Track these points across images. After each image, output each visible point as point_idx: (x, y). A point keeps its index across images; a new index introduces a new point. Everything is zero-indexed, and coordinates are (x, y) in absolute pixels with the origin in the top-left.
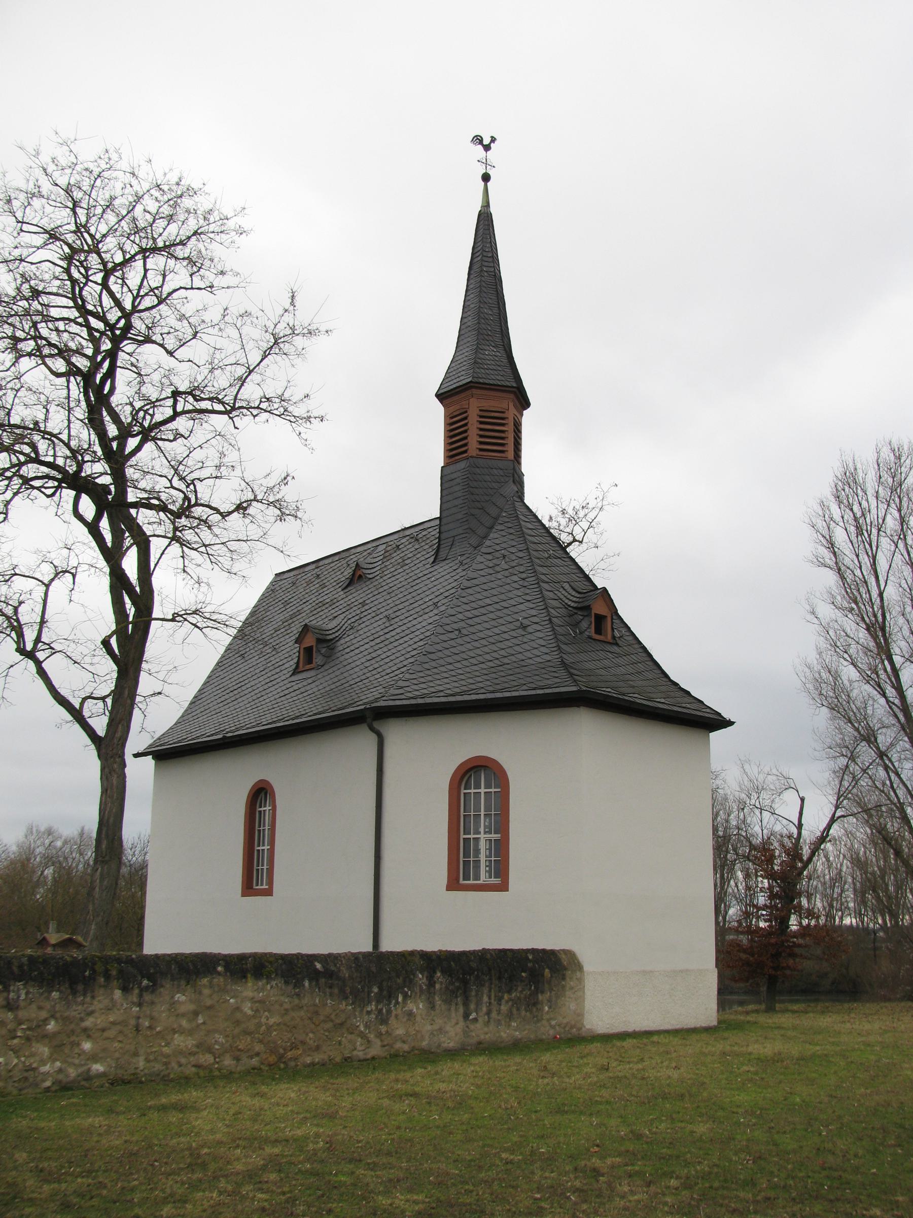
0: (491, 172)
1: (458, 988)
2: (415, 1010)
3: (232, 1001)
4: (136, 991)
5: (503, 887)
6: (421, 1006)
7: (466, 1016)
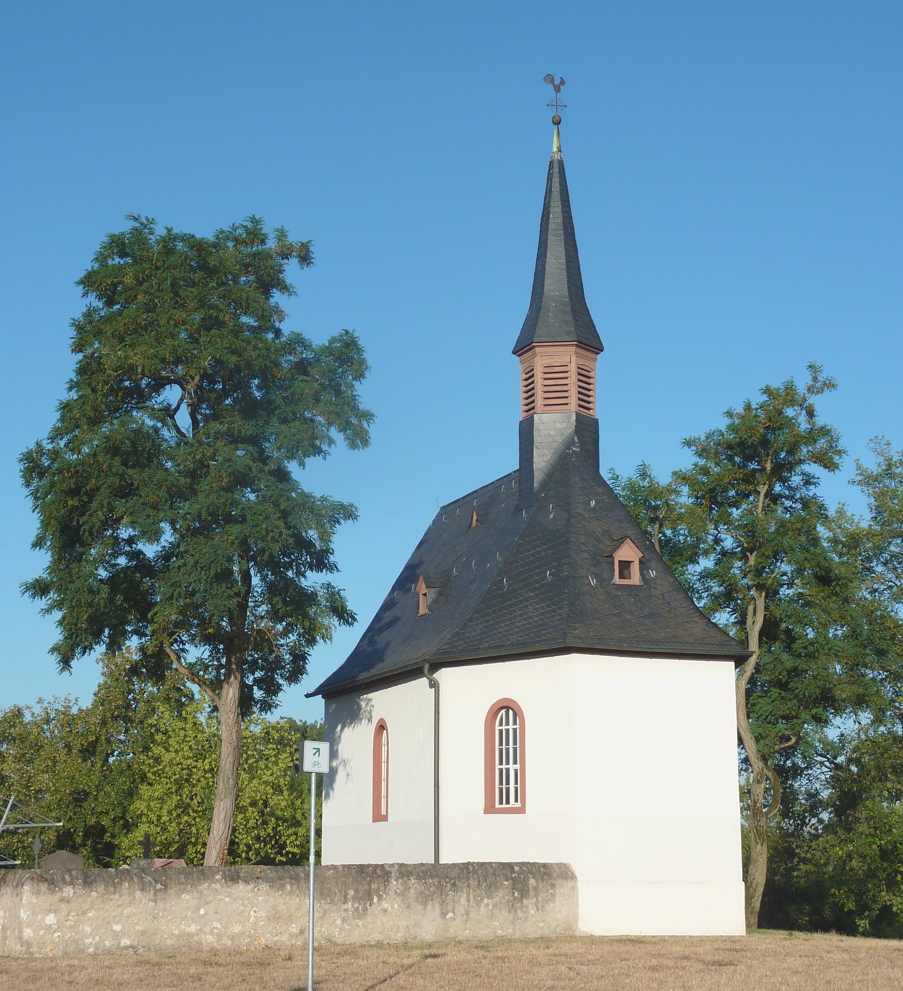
0: (563, 114)
4: (152, 892)
5: (522, 810)
6: (396, 906)
7: (444, 914)
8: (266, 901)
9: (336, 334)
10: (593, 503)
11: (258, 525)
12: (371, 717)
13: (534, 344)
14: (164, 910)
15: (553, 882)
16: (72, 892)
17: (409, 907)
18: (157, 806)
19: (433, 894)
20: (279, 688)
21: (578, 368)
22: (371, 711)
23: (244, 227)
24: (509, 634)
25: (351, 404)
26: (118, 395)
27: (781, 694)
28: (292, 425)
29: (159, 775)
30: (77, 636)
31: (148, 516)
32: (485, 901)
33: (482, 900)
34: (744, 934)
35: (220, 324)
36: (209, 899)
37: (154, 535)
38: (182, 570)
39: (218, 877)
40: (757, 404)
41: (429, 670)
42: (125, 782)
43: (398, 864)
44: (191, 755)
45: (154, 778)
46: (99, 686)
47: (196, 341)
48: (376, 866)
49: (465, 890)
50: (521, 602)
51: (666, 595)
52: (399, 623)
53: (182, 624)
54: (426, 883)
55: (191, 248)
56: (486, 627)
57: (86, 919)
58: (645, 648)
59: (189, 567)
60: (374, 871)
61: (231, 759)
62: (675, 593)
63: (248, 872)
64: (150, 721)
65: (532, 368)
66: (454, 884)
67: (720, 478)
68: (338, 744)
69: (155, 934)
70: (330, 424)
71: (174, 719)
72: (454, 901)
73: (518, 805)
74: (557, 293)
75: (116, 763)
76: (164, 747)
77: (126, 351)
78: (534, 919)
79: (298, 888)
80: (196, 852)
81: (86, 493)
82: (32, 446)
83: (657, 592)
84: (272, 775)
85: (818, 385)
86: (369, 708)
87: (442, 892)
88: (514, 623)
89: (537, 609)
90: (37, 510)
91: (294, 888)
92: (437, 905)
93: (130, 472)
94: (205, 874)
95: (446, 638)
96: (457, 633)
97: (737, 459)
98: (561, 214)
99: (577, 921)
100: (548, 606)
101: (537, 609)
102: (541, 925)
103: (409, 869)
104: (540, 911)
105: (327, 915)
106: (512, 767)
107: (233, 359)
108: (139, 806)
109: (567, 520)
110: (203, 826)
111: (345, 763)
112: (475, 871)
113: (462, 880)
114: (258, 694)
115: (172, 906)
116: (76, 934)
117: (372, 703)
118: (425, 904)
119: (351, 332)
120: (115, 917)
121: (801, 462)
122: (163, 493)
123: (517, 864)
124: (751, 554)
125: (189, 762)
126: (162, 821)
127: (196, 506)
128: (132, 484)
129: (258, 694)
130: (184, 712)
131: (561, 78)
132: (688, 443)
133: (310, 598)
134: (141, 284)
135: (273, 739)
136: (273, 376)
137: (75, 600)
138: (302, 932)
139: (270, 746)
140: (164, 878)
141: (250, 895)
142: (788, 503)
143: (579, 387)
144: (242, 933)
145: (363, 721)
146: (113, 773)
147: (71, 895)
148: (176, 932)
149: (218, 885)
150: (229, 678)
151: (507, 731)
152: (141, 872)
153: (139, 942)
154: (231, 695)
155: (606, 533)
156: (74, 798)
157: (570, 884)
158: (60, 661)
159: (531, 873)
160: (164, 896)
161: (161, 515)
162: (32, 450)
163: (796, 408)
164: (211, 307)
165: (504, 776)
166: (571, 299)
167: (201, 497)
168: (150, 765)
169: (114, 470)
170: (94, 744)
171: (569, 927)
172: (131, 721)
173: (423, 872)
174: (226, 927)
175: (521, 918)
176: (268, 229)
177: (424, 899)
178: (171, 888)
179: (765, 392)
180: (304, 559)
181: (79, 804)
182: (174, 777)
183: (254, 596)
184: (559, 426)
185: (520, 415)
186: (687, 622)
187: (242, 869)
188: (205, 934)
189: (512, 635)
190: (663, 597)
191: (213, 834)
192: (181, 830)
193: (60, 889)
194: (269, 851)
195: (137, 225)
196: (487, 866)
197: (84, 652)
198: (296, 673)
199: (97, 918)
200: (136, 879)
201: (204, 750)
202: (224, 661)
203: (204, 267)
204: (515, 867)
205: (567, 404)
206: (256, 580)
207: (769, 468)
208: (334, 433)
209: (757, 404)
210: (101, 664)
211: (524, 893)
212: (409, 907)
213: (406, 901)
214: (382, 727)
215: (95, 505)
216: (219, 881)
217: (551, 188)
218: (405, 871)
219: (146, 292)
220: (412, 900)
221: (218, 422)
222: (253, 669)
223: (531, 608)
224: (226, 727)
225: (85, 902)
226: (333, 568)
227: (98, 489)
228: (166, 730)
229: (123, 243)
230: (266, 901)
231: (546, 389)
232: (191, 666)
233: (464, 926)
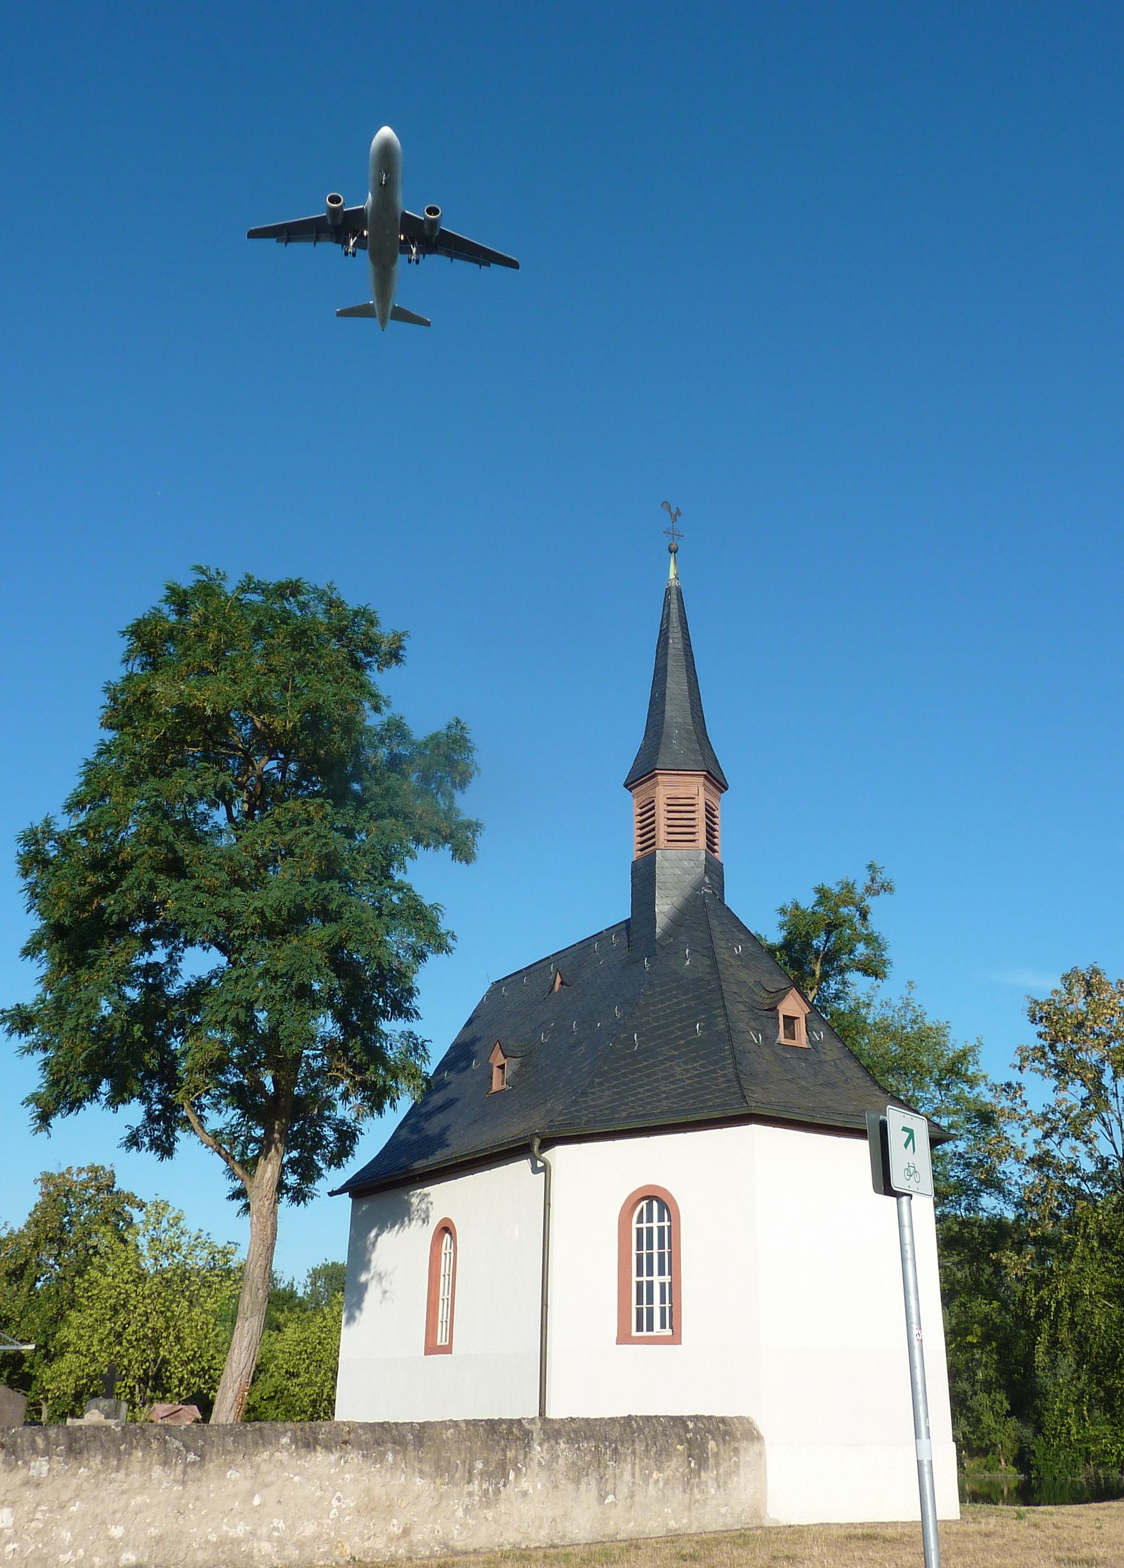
1: (590, 1464)
2: (531, 1491)
4: (180, 1468)
5: (675, 1339)
6: (539, 1486)
7: (602, 1498)
12: (428, 1217)
13: (657, 771)
14: (197, 1499)
15: (736, 1445)
16: (45, 1468)
17: (556, 1487)
22: (428, 1208)
24: (655, 1101)
30: (66, 1084)
33: (651, 1474)
36: (269, 1479)
39: (285, 1440)
46: (36, 1205)
49: (629, 1459)
50: (662, 1062)
51: (838, 1062)
52: (458, 1104)
54: (579, 1449)
57: (66, 1516)
60: (510, 1431)
63: (330, 1432)
68: (371, 1253)
69: (179, 1542)
74: (680, 720)
78: (714, 1502)
81: (114, 869)
82: (38, 823)
85: (875, 886)
90: (33, 911)
91: (399, 1458)
92: (593, 1483)
99: (765, 1503)
101: (687, 1070)
102: (723, 1510)
103: (557, 1426)
104: (722, 1489)
105: (444, 1503)
106: (657, 1279)
108: (66, 1334)
111: (380, 1277)
112: (640, 1430)
113: (626, 1445)
115: (210, 1492)
116: (45, 1545)
118: (577, 1482)
120: (114, 1513)
123: (690, 1418)
137: (85, 1014)
138: (406, 1532)
140: (201, 1443)
141: (333, 1471)
144: (317, 1537)
148: (213, 1538)
149: (285, 1454)
150: (269, 1151)
151: (650, 1231)
152: (163, 1432)
153: (150, 1556)
154: (268, 1175)
157: (756, 1447)
158: (38, 1117)
159: (709, 1431)
160: (198, 1474)
162: (37, 828)
165: (644, 1293)
170: (23, 1267)
173: (574, 1431)
174: (292, 1528)
175: (698, 1501)
177: (577, 1474)
178: (211, 1461)
187: (321, 1427)
188: (259, 1539)
189: (659, 1101)
193: (26, 1463)
194: (202, 1386)
195: (204, 578)
197: (71, 1110)
199: (84, 1515)
200: (155, 1445)
204: (689, 1423)
207: (818, 973)
211: (702, 1463)
213: (553, 1478)
216: (286, 1448)
220: (560, 1476)
223: (678, 1069)
224: (258, 1218)
225: (65, 1486)
230: (355, 1481)
231: (670, 823)
233: (627, 1516)
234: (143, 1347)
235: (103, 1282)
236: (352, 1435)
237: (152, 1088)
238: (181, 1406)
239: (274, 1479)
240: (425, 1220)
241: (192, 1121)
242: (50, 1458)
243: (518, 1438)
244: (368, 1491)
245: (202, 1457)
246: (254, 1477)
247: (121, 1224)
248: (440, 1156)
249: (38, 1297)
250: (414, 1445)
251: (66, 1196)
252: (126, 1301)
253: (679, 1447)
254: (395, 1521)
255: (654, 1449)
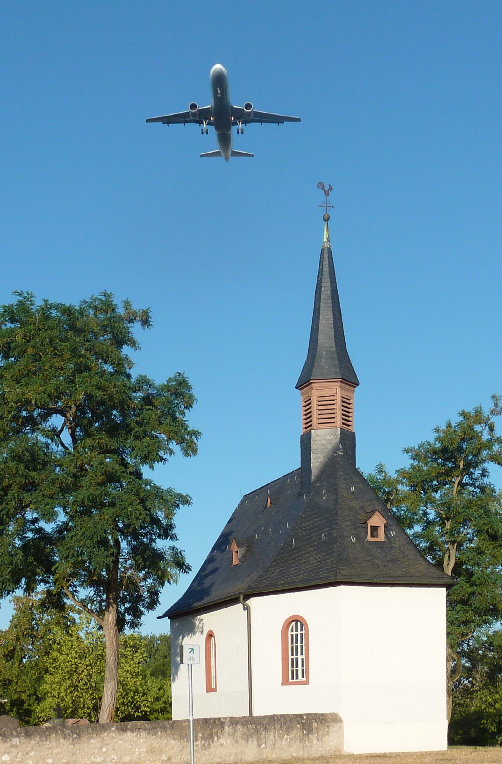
2: (225, 744)
3: (119, 742)
4: (71, 740)
5: (307, 683)
6: (229, 742)
7: (259, 745)
8: (144, 742)
9: (172, 376)
10: (353, 489)
11: (125, 508)
12: (203, 630)
13: (311, 381)
15: (328, 724)
16: (18, 741)
17: (237, 742)
18: (57, 686)
19: (252, 734)
20: (142, 613)
21: (342, 397)
22: (203, 626)
23: (99, 300)
25: (183, 426)
26: (19, 421)
27: (463, 608)
28: (144, 440)
29: (57, 669)
31: (48, 504)
32: (285, 737)
33: (283, 736)
34: (447, 749)
35: (88, 368)
36: (108, 742)
37: (50, 516)
38: (74, 539)
39: (113, 729)
40: (456, 423)
41: (243, 599)
42: (35, 673)
43: (229, 717)
44: (77, 656)
45: (53, 670)
46: (13, 616)
47: (73, 382)
48: (215, 719)
49: (272, 731)
50: (305, 554)
53: (73, 575)
54: (247, 728)
55: (63, 314)
56: (281, 571)
57: (29, 756)
58: (389, 581)
59: (78, 537)
60: (214, 722)
61: (113, 658)
62: (407, 546)
64: (48, 637)
65: (310, 398)
66: (266, 728)
67: (429, 473)
70: (170, 439)
71: (64, 635)
72: (265, 738)
73: (304, 679)
74: (327, 345)
75: (28, 663)
76: (59, 652)
77: (22, 389)
78: (316, 746)
79: (166, 733)
80: (84, 713)
83: (396, 546)
84: (130, 666)
86: (201, 625)
87: (258, 733)
88: (300, 568)
89: (316, 559)
92: (255, 741)
93: (33, 474)
94: (104, 728)
95: (254, 579)
96: (262, 576)
97: (440, 461)
98: (330, 288)
99: (343, 746)
100: (323, 556)
101: (316, 559)
103: (237, 720)
104: (320, 741)
107: (99, 394)
108: (45, 687)
109: (336, 500)
110: (88, 698)
113: (270, 725)
114: (128, 617)
117: (203, 622)
118: (247, 740)
119: (182, 373)
120: (48, 755)
121: (483, 461)
122: (55, 489)
123: (305, 715)
124: (448, 521)
125: (76, 660)
126: (61, 695)
127: (81, 497)
128: (34, 482)
129: (128, 617)
130: (70, 631)
131: (330, 185)
132: (407, 451)
133: (159, 556)
134: (29, 341)
135: (130, 645)
136: (128, 407)
139: (128, 649)
140: (78, 731)
141: (135, 739)
142: (471, 489)
143: (343, 410)
145: (197, 633)
146: (27, 668)
147: (18, 743)
149: (114, 733)
150: (109, 607)
154: (110, 618)
155: (362, 508)
156: (3, 684)
157: (339, 725)
159: (314, 719)
160: (79, 741)
161: (57, 502)
163: (482, 425)
164: (80, 356)
166: (337, 349)
167: (83, 491)
168: (51, 663)
169: (20, 472)
171: (338, 750)
172: (35, 637)
173: (245, 721)
174: (120, 758)
175: (308, 746)
176: (117, 301)
177: (247, 737)
178: (83, 737)
179: (461, 415)
180: (155, 530)
181: (6, 687)
182: (67, 669)
183: (122, 555)
184: (329, 437)
185: (302, 431)
186: (416, 564)
187: (128, 724)
189: (299, 575)
190: (400, 548)
191: (104, 703)
192: (74, 701)
193: (11, 740)
195: (22, 298)
196: (286, 716)
198: (153, 604)
200: (59, 732)
201: (84, 653)
202: (104, 597)
203: (73, 328)
205: (334, 422)
206: (123, 544)
207: (462, 467)
208: (173, 445)
209: (456, 423)
210: (12, 603)
212: (237, 742)
214: (210, 635)
215: (9, 497)
217: (322, 269)
218: (234, 721)
219: (34, 347)
220: (239, 738)
221: (91, 439)
222: (124, 600)
223: (312, 558)
224: (109, 638)
226: (173, 537)
227: (10, 486)
228: (59, 641)
229: (13, 312)
230: (144, 742)
231: (320, 412)
232: (82, 601)
234: (91, 692)
235: (61, 658)
236: (142, 726)
237: (49, 577)
238: (80, 719)
239: (110, 742)
240: (202, 632)
241: (69, 595)
242: (19, 738)
243: (218, 725)
244: (151, 745)
245: (79, 735)
246: (102, 742)
247: (69, 623)
248: (207, 600)
249: (25, 667)
250: (170, 728)
251: (31, 609)
252: (77, 668)
253: (298, 726)
254: (164, 755)
255: (285, 727)
